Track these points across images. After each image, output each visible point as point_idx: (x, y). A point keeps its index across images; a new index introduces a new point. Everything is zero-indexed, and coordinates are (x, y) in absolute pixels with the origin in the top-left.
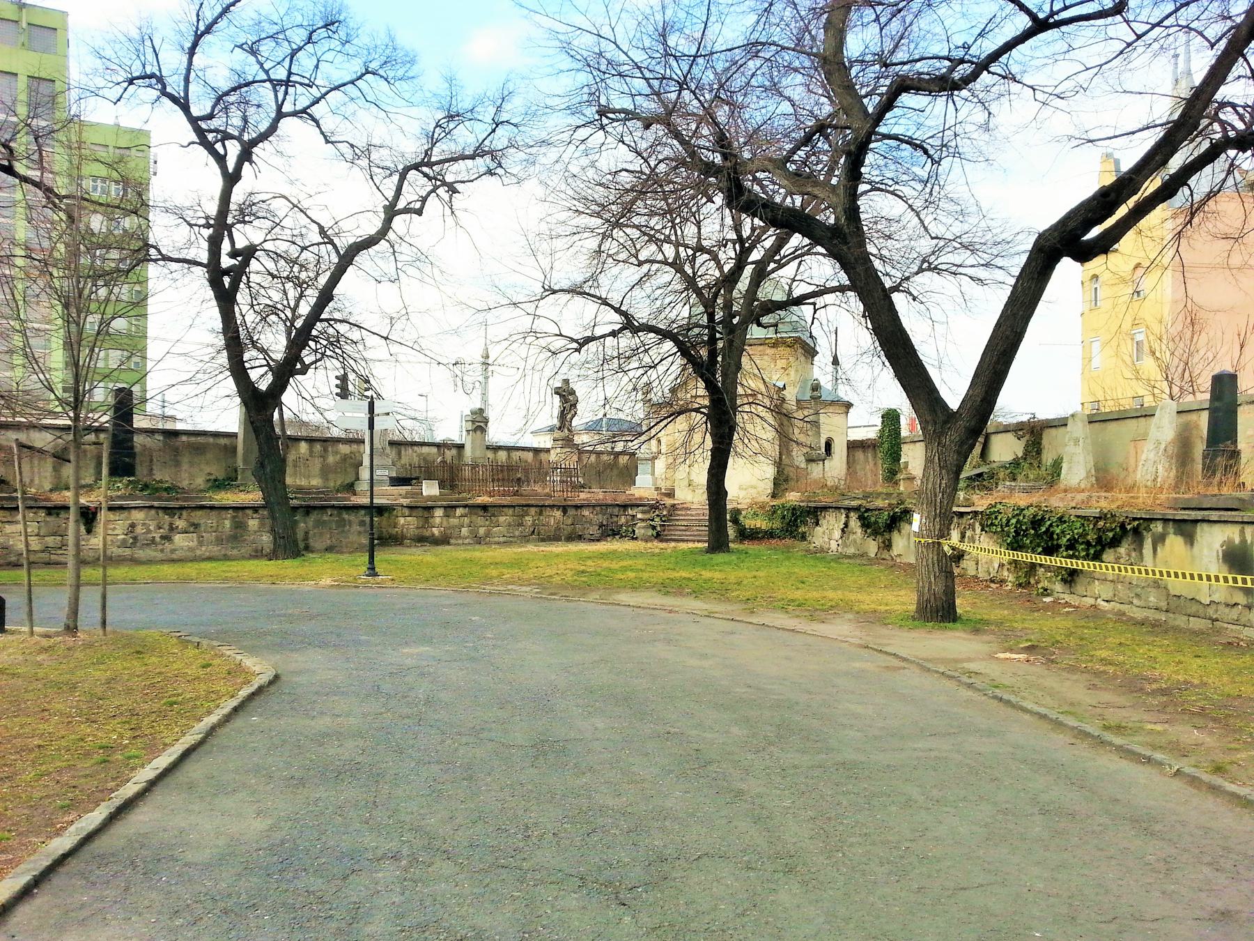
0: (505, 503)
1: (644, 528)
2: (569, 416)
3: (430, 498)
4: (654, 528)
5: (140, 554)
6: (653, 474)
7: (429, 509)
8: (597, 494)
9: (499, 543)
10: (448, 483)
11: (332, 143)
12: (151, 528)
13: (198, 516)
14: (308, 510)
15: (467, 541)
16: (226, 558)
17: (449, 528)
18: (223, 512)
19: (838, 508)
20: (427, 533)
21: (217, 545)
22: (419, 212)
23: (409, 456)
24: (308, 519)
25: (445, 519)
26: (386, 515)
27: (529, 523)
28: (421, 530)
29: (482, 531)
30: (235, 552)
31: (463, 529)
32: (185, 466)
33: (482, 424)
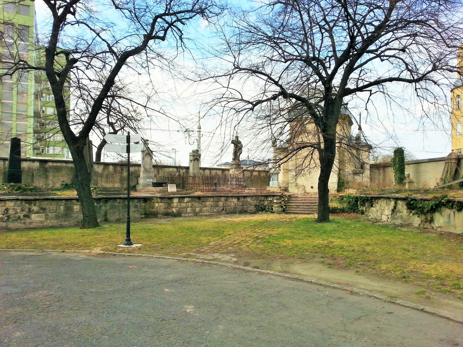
0: (209, 195)
1: (278, 207)
2: (239, 154)
3: (173, 193)
4: (282, 207)
5: (11, 225)
6: (278, 181)
7: (171, 199)
8: (253, 190)
9: (206, 215)
10: (181, 185)
11: (120, 9)
12: (18, 211)
13: (45, 204)
14: (106, 200)
15: (190, 215)
16: (61, 227)
17: (182, 208)
18: (60, 202)
19: (388, 198)
20: (170, 211)
21: (56, 220)
22: (163, 39)
23: (162, 173)
24: (106, 205)
25: (179, 204)
26: (149, 202)
27: (221, 205)
28: (166, 210)
29: (198, 209)
30: (66, 223)
31: (188, 209)
32: (51, 178)
33: (198, 157)
